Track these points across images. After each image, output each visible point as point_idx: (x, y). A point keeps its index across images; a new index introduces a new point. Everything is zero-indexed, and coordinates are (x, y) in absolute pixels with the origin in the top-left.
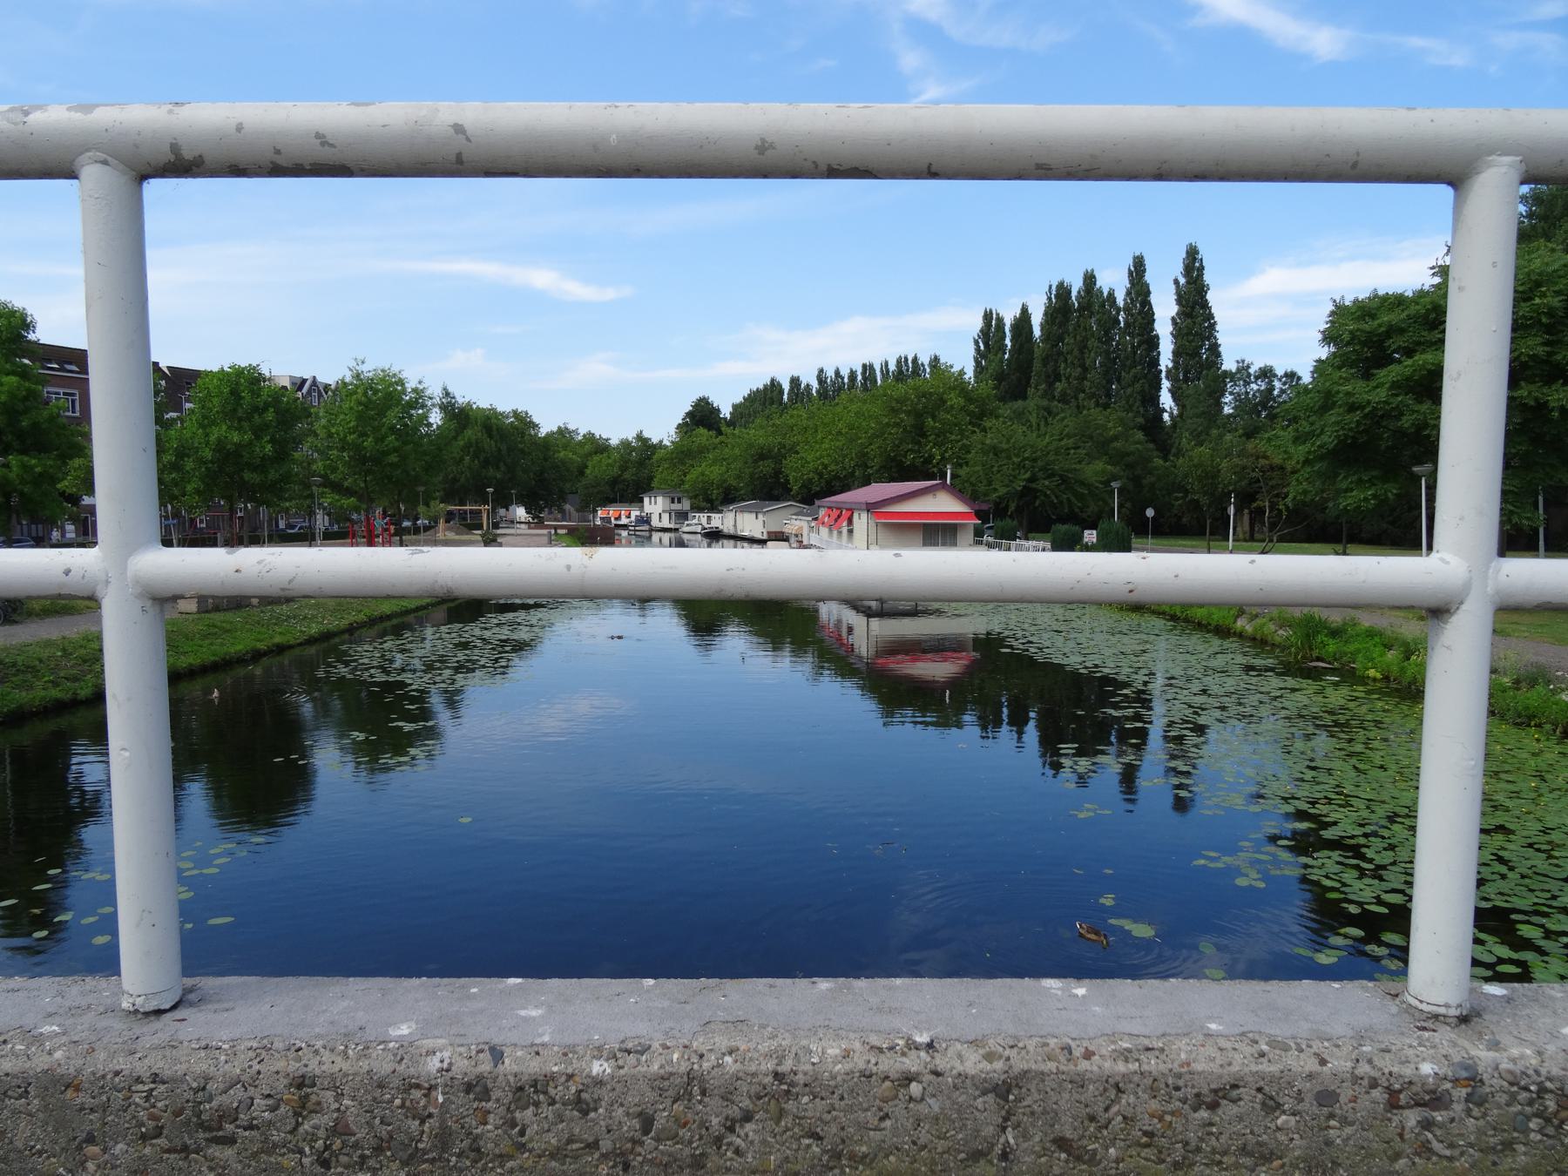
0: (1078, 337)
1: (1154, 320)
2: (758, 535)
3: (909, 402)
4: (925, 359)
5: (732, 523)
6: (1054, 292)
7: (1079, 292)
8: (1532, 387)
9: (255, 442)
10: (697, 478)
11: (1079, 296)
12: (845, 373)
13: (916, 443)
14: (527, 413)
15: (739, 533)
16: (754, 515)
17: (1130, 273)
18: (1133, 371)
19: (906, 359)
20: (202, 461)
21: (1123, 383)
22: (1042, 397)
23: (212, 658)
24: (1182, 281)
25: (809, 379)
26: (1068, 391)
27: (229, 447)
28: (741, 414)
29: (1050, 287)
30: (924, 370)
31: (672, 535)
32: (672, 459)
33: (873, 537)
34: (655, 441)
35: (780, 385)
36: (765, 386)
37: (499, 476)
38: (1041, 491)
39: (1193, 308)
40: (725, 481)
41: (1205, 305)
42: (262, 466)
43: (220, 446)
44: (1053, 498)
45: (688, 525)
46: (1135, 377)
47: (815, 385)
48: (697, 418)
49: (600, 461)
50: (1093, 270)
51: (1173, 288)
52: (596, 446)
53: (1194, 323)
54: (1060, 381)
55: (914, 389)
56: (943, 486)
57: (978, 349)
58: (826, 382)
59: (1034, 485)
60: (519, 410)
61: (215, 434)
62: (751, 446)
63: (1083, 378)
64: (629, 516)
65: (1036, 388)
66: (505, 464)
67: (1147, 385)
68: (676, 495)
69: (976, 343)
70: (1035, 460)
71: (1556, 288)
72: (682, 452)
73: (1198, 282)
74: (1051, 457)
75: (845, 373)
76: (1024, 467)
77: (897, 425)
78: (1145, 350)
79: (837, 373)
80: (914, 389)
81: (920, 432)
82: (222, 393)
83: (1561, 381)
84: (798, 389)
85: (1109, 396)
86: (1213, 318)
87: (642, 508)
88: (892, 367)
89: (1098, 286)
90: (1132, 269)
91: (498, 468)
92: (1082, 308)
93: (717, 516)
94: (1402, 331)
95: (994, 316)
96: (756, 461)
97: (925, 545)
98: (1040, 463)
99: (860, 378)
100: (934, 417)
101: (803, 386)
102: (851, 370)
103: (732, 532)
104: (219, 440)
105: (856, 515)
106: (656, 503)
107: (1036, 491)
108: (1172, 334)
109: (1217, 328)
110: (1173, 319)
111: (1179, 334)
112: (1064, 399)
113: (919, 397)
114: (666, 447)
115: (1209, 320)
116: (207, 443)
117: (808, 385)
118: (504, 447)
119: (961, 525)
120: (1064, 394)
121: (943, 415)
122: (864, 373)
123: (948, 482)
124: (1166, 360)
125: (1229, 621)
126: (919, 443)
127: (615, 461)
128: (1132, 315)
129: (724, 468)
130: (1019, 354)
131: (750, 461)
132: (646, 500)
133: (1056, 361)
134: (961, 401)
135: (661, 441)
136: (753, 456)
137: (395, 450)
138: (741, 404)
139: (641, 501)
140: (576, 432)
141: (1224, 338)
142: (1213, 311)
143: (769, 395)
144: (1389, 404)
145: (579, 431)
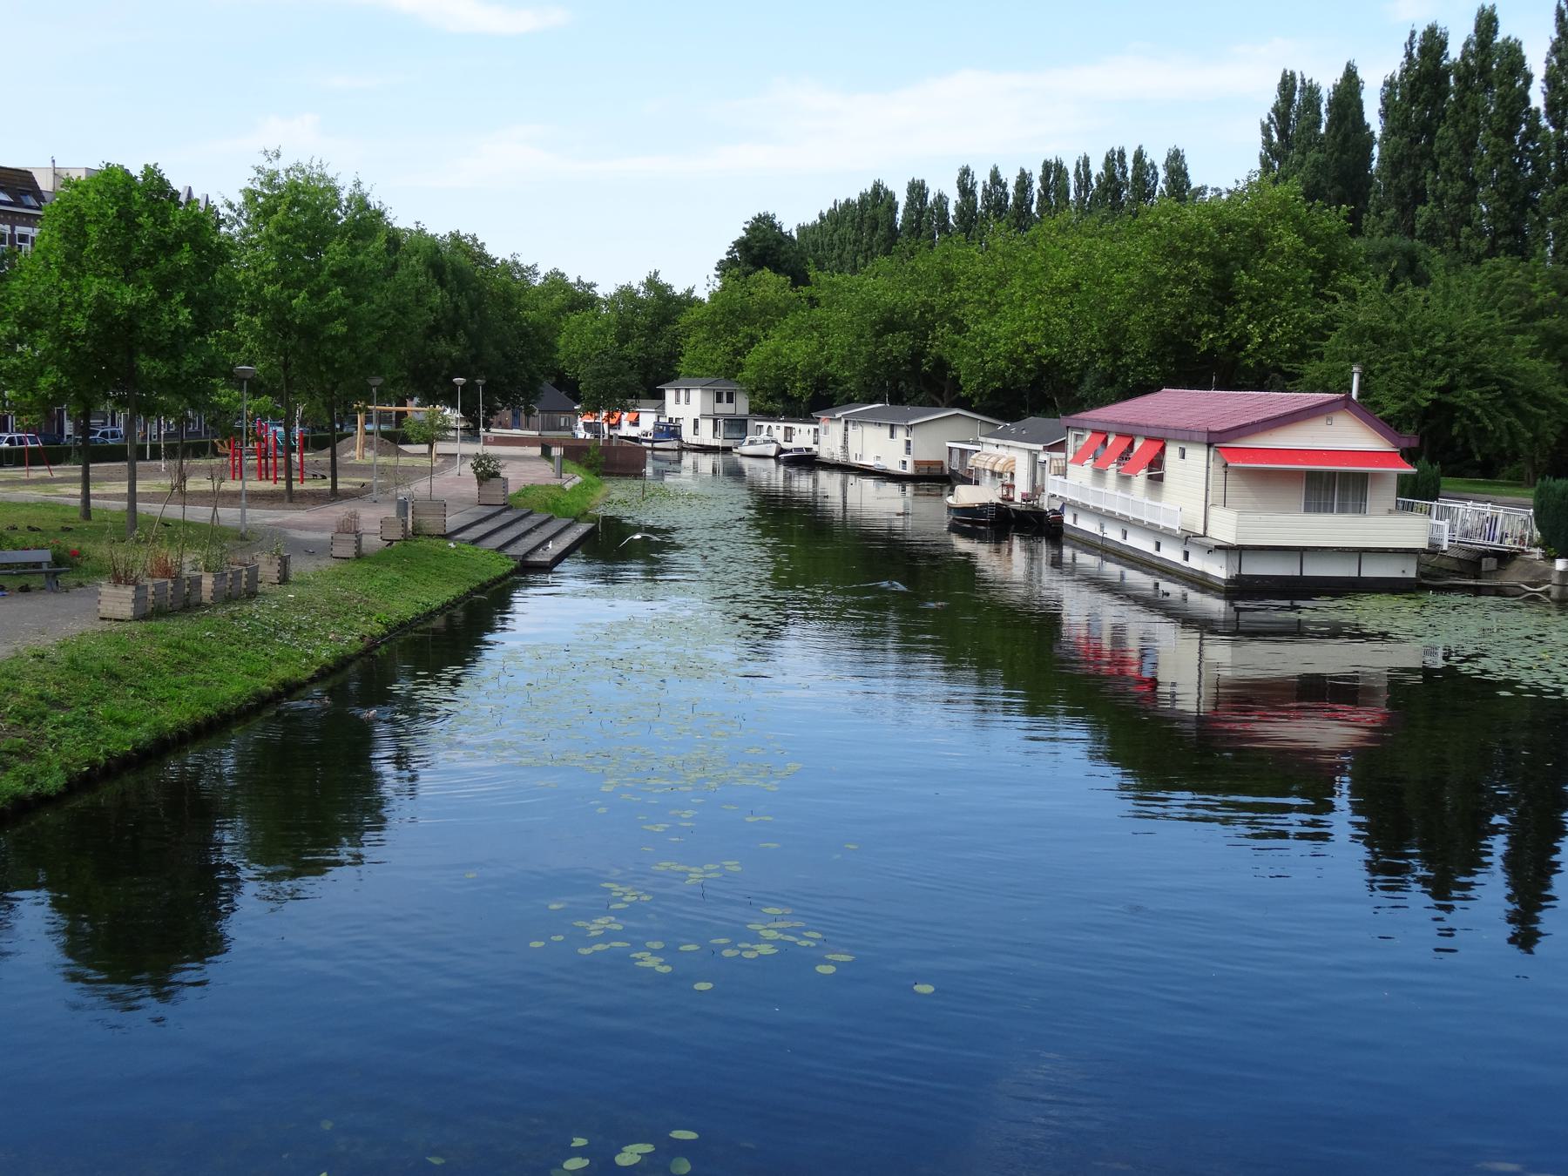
0: (1461, 127)
2: (895, 467)
4: (1157, 157)
5: (840, 442)
6: (1417, 45)
7: (1466, 45)
9: (160, 305)
10: (767, 359)
12: (1010, 179)
13: (1215, 314)
14: (475, 239)
15: (853, 461)
16: (886, 431)
19: (1122, 154)
20: (66, 337)
23: (206, 711)
25: (943, 185)
26: (1441, 222)
27: (118, 312)
28: (815, 244)
29: (1413, 34)
30: (1156, 174)
31: (719, 459)
32: (713, 324)
33: (1216, 493)
34: (679, 290)
35: (890, 196)
36: (863, 196)
37: (455, 353)
38: (1464, 408)
40: (818, 366)
42: (171, 349)
43: (102, 310)
44: (1487, 421)
45: (751, 443)
47: (954, 197)
48: (755, 251)
49: (582, 324)
50: (1493, 7)
52: (580, 300)
54: (1425, 203)
55: (1213, 217)
56: (1347, 404)
57: (1268, 143)
58: (972, 192)
59: (1450, 399)
60: (462, 234)
61: (94, 287)
62: (871, 306)
64: (635, 423)
65: (1378, 214)
66: (467, 333)
68: (725, 388)
69: (1266, 130)
70: (1450, 353)
72: (732, 312)
74: (1483, 348)
75: (1010, 179)
76: (1432, 365)
77: (1181, 280)
79: (995, 177)
80: (1213, 217)
81: (1222, 293)
82: (104, 215)
84: (923, 202)
87: (660, 410)
88: (1097, 168)
91: (453, 339)
93: (805, 427)
95: (1299, 84)
96: (879, 335)
97: (1307, 509)
98: (1461, 359)
99: (1037, 185)
101: (931, 198)
102: (1023, 172)
103: (838, 457)
104: (98, 297)
105: (1172, 452)
106: (688, 401)
107: (1453, 408)
112: (1432, 235)
113: (1222, 231)
114: (701, 302)
116: (79, 306)
117: (940, 196)
118: (464, 304)
119: (1376, 475)
123: (1354, 395)
126: (1221, 313)
127: (609, 325)
129: (814, 343)
130: (1343, 152)
131: (868, 333)
132: (670, 395)
133: (1418, 168)
134: (1300, 242)
135: (690, 291)
136: (874, 324)
137: (342, 311)
138: (814, 226)
139: (660, 396)
140: (533, 270)
143: (869, 212)
145: (538, 269)
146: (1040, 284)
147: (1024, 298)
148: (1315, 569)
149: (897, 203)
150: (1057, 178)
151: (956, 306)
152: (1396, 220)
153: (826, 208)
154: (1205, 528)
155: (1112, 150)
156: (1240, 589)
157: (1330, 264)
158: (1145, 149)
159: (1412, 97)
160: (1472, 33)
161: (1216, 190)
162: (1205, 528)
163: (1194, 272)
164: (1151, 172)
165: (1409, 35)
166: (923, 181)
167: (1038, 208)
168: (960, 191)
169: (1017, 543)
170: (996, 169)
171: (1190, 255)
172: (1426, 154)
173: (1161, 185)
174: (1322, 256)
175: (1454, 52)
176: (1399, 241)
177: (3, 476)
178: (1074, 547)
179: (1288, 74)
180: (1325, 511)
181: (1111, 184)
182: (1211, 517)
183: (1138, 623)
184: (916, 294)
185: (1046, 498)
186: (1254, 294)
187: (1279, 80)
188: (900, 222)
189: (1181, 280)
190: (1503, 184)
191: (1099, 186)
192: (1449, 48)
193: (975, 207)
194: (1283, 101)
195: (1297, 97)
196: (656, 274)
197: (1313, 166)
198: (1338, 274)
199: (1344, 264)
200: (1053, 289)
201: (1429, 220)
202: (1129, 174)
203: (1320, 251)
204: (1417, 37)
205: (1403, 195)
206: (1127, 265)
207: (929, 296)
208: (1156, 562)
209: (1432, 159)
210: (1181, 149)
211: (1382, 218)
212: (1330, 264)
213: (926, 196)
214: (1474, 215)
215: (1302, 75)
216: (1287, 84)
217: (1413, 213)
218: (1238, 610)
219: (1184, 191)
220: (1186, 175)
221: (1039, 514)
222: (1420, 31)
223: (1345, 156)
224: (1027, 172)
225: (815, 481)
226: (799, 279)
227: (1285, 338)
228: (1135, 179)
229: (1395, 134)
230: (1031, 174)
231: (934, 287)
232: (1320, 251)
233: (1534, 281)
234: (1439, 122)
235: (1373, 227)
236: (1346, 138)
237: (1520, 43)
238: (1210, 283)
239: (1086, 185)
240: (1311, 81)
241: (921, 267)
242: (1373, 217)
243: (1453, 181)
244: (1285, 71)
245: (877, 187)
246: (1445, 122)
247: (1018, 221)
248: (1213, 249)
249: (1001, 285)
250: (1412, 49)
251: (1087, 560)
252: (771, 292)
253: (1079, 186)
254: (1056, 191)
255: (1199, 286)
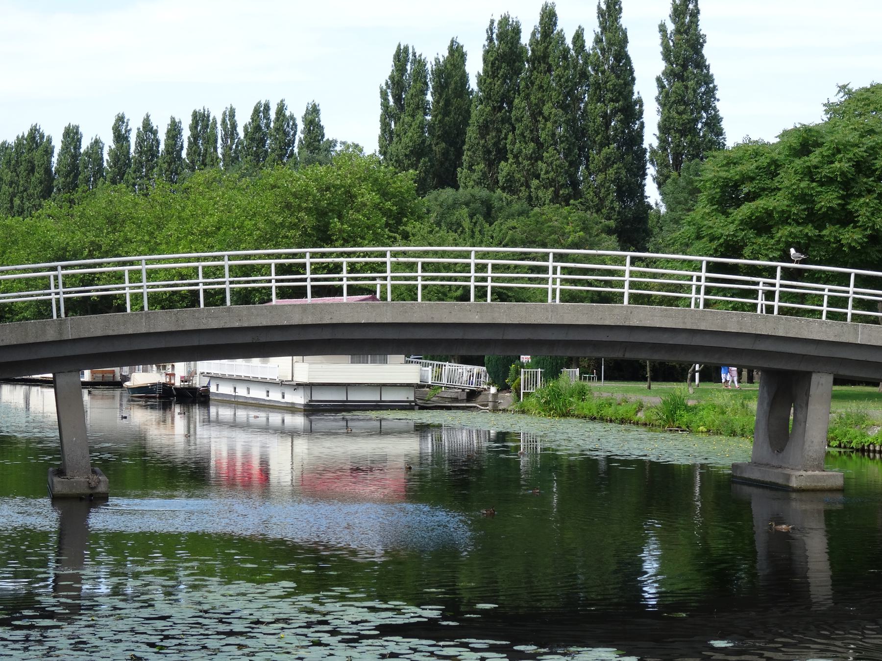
1: (633, 79)
3: (310, 198)
4: (297, 111)
6: (496, 31)
7: (534, 34)
8: (833, 228)
11: (534, 42)
17: (601, 13)
18: (605, 150)
19: (267, 108)
21: (591, 166)
22: (478, 183)
24: (671, 27)
26: (517, 176)
29: (492, 22)
30: (295, 125)
36: (19, 142)
39: (684, 67)
41: (701, 64)
46: (608, 159)
47: (108, 142)
51: (657, 38)
53: (686, 87)
63: (536, 157)
65: (470, 168)
67: (624, 172)
69: (384, 95)
71: (848, 156)
73: (692, 31)
78: (621, 121)
80: (316, 180)
83: (852, 225)
84: (78, 147)
85: (575, 184)
86: (712, 81)
88: (243, 119)
89: (558, 28)
90: (604, 7)
92: (534, 60)
94: (752, 179)
95: (410, 56)
97: (352, 363)
99: (186, 134)
100: (340, 217)
108: (657, 99)
109: (718, 95)
110: (659, 80)
111: (665, 101)
112: (510, 187)
113: (320, 190)
115: (707, 84)
120: (510, 179)
121: (352, 215)
122: (193, 127)
124: (651, 139)
125: (630, 414)
128: (603, 72)
133: (499, 131)
134: (377, 198)
141: (724, 106)
142: (711, 72)
143: (26, 156)
144: (736, 237)
146: (191, 227)
147: (179, 239)
149: (54, 147)
151: (120, 245)
152: (484, 174)
154: (293, 376)
155: (259, 103)
157: (402, 213)
158: (286, 103)
159: (493, 73)
160: (538, 24)
161: (343, 143)
162: (293, 376)
163: (301, 220)
164: (291, 123)
165: (489, 23)
166: (78, 127)
167: (188, 154)
168: (115, 137)
169: (177, 409)
170: (148, 116)
171: (300, 208)
172: (506, 120)
174: (395, 208)
175: (525, 39)
176: (482, 193)
177: (2, 272)
178: (217, 406)
179: (402, 47)
180: (363, 363)
182: (295, 369)
184: (84, 234)
185: (198, 378)
186: (345, 235)
187: (394, 52)
188: (55, 165)
190: (562, 145)
191: (246, 135)
192: (522, 35)
193: (128, 152)
194: (397, 71)
195: (408, 67)
197: (419, 127)
198: (408, 221)
199: (412, 213)
200: (201, 232)
201: (508, 174)
203: (394, 205)
204: (496, 24)
206: (255, 214)
207: (96, 236)
208: (267, 403)
209: (511, 124)
210: (317, 104)
211: (474, 171)
212: (402, 213)
213: (79, 140)
214: (541, 170)
215: (413, 49)
216: (401, 56)
217: (497, 167)
218: (311, 422)
219: (319, 141)
221: (193, 390)
223: (447, 118)
224: (177, 120)
227: (367, 267)
229: (481, 103)
230: (180, 122)
231: (101, 230)
232: (394, 205)
233: (568, 224)
234: (514, 93)
235: (466, 178)
236: (448, 103)
237: (583, 29)
238: (313, 228)
239: (232, 134)
240: (420, 56)
241: (90, 212)
242: (465, 170)
243: (526, 143)
244: (399, 45)
245: (34, 132)
246: (519, 94)
247: (169, 165)
248: (316, 205)
249: (159, 227)
250: (492, 34)
251: (226, 413)
253: (226, 134)
254: (204, 139)
255: (306, 230)
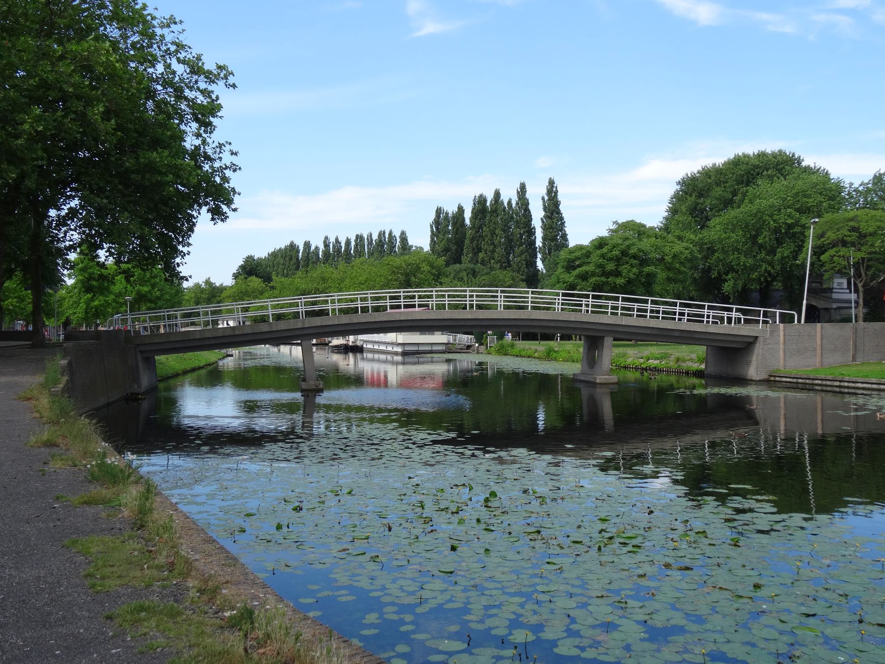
19: (384, 232)
26: (486, 259)
29: (475, 197)
30: (396, 239)
47: (322, 247)
57: (432, 231)
58: (329, 246)
69: (431, 227)
77: (396, 280)
79: (337, 240)
88: (375, 237)
99: (353, 243)
143: (289, 253)
147: (350, 286)
148: (421, 348)
150: (361, 241)
153: (271, 250)
156: (404, 354)
173: (398, 243)
181: (380, 242)
183: (382, 367)
189: (396, 280)
191: (376, 244)
196: (209, 278)
202: (387, 240)
203: (436, 271)
205: (474, 249)
213: (310, 247)
220: (407, 240)
221: (357, 347)
222: (478, 195)
225: (279, 350)
226: (267, 279)
228: (389, 241)
232: (436, 271)
236: (457, 230)
238: (404, 281)
245: (292, 243)
249: (343, 281)
251: (370, 356)
252: (256, 285)
